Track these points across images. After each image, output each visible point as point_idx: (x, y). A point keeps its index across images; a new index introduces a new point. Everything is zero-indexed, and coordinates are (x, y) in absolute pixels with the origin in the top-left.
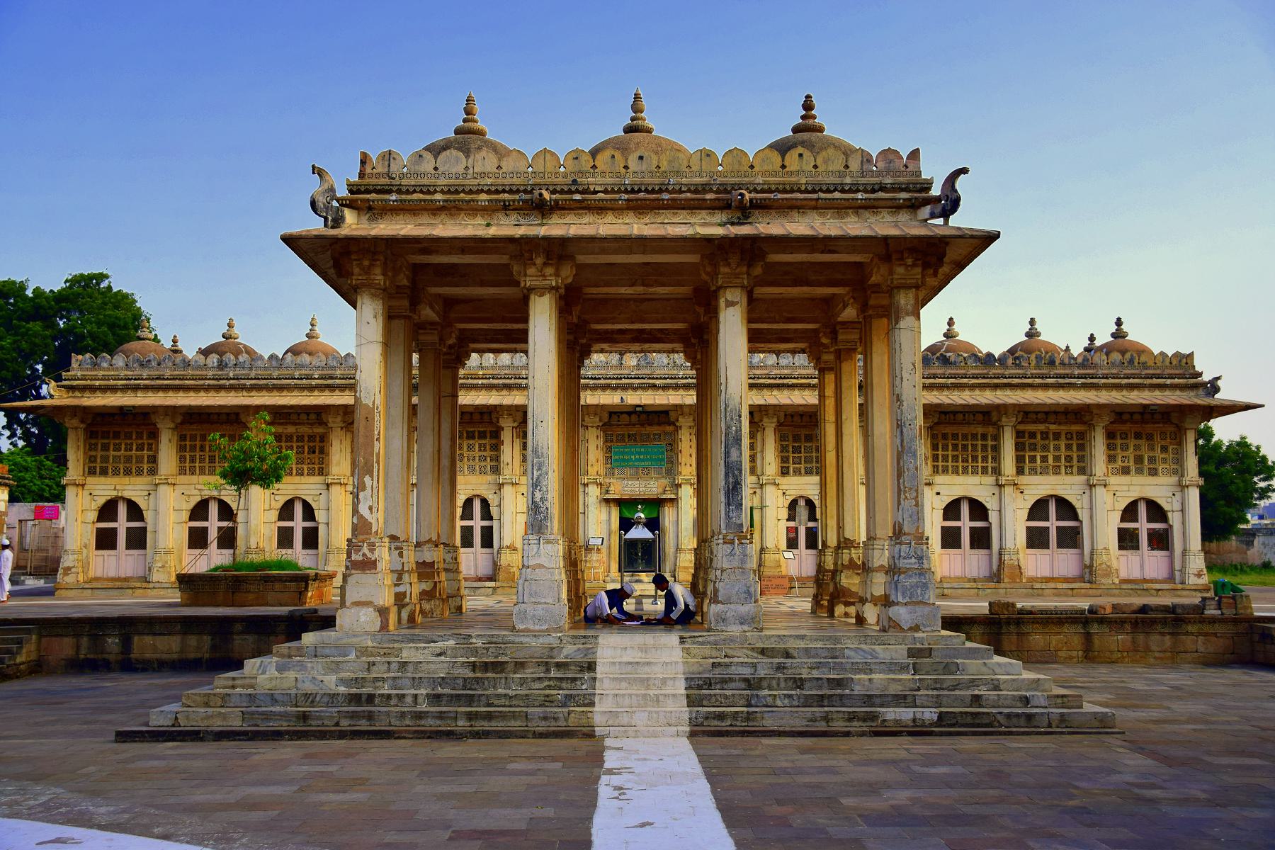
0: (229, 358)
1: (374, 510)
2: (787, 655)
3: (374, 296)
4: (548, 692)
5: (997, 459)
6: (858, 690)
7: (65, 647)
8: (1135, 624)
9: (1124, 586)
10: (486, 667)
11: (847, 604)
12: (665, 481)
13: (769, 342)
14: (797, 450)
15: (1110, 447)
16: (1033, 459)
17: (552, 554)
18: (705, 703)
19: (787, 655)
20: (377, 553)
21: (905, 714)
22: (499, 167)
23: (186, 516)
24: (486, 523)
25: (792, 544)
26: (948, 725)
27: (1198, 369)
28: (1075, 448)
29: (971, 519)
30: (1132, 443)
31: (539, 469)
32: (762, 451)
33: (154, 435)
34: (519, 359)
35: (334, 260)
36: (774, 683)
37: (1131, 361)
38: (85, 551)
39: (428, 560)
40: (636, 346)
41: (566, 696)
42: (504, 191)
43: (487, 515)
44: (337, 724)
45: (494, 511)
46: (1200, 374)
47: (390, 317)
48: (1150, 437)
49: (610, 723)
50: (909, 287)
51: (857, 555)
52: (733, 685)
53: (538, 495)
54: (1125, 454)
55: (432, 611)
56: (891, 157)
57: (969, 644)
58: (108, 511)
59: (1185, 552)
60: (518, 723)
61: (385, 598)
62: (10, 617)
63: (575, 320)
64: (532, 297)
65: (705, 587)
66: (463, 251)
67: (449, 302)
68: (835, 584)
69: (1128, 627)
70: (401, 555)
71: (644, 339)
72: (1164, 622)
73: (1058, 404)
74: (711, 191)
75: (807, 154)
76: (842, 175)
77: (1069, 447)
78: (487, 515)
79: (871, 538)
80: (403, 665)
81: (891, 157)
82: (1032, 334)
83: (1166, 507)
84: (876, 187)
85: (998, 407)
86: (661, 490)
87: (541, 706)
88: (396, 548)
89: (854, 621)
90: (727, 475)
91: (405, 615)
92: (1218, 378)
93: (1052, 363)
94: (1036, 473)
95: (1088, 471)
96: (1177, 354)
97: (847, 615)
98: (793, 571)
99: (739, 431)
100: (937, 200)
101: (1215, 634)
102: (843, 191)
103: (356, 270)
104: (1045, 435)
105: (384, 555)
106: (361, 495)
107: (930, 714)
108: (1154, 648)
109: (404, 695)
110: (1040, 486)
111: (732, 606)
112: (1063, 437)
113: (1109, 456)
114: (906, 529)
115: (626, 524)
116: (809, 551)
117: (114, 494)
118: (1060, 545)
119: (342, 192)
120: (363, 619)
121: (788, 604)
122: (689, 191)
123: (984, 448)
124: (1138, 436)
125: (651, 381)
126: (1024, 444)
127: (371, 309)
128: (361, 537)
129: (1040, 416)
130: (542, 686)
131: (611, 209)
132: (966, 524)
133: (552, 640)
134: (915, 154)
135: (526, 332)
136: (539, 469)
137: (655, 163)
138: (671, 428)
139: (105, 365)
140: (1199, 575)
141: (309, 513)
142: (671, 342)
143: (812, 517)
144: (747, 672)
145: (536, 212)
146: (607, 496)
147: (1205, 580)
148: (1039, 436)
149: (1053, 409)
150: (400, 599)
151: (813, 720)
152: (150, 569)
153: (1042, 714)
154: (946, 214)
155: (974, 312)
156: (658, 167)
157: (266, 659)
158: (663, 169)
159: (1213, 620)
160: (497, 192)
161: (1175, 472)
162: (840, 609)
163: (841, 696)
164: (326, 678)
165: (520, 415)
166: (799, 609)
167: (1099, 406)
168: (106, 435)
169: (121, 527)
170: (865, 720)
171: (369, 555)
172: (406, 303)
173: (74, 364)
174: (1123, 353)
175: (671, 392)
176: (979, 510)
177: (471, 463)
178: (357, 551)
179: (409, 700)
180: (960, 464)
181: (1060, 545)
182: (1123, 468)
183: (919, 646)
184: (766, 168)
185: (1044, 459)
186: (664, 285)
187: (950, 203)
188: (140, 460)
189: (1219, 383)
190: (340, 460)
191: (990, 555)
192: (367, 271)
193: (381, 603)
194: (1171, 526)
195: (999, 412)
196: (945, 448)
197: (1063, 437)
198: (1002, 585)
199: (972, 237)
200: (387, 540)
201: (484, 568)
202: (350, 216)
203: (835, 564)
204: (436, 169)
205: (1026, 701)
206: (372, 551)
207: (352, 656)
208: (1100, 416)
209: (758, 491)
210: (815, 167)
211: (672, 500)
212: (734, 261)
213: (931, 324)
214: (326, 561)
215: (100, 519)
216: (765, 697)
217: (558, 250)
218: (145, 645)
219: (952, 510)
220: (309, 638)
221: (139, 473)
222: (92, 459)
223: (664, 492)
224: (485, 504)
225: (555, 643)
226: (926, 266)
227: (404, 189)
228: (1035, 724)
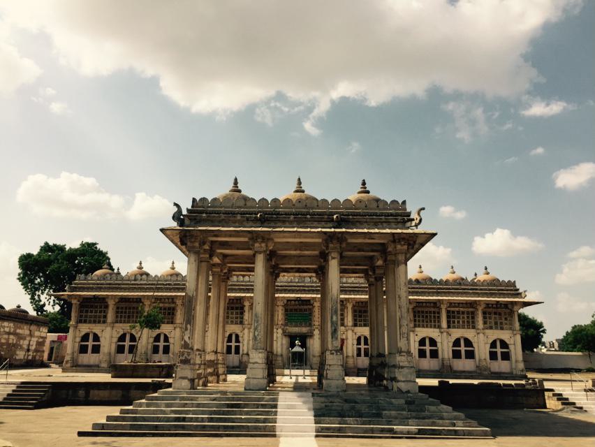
16: (454, 322)
20: (190, 356)
22: (245, 205)
24: (237, 344)
27: (518, 287)
30: (493, 316)
45: (241, 339)
46: (518, 290)
48: (500, 314)
59: (516, 361)
66: (230, 236)
67: (225, 256)
70: (201, 357)
77: (468, 317)
78: (237, 340)
88: (199, 354)
99: (337, 308)
104: (458, 312)
118: (466, 358)
119: (185, 212)
120: (183, 384)
123: (434, 317)
124: (495, 313)
134: (404, 202)
138: (311, 307)
168: (87, 307)
172: (208, 256)
181: (466, 358)
185: (458, 322)
186: (307, 250)
196: (419, 317)
222: (81, 316)
224: (237, 336)
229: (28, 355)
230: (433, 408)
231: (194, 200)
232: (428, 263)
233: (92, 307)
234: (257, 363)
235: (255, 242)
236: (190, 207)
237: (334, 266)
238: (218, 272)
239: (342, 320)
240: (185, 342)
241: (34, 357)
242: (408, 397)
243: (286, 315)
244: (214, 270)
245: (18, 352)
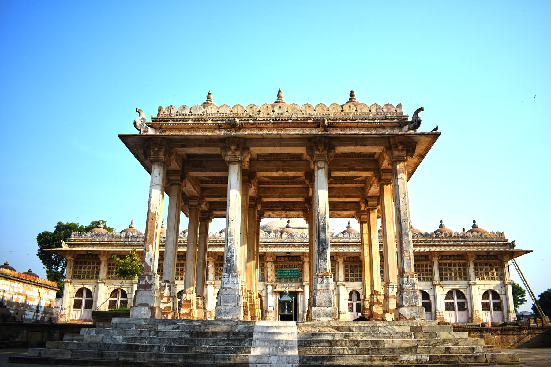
0: (130, 234)
1: (152, 260)
2: (350, 330)
3: (159, 165)
5: (432, 274)
10: (198, 334)
12: (298, 284)
13: (339, 210)
14: (352, 271)
15: (476, 269)
16: (446, 275)
27: (506, 238)
28: (462, 270)
30: (484, 267)
32: (338, 272)
33: (99, 263)
36: (344, 343)
37: (481, 235)
44: (118, 359)
46: (507, 240)
48: (491, 265)
49: (258, 361)
52: (322, 344)
54: (482, 272)
56: (389, 107)
60: (210, 361)
67: (211, 203)
76: (367, 113)
77: (460, 269)
80: (157, 332)
81: (389, 107)
82: (441, 226)
84: (384, 118)
85: (431, 253)
87: (223, 353)
90: (319, 245)
92: (514, 241)
93: (451, 236)
94: (448, 280)
96: (498, 232)
100: (412, 122)
102: (369, 120)
103: (152, 153)
104: (450, 265)
108: (510, 341)
109: (153, 346)
111: (323, 308)
113: (476, 273)
120: (143, 312)
123: (427, 270)
124: (486, 265)
128: (145, 273)
129: (448, 257)
130: (225, 344)
134: (399, 106)
136: (230, 242)
137: (286, 110)
138: (301, 263)
139: (83, 236)
142: (298, 211)
143: (359, 299)
144: (329, 338)
149: (452, 254)
151: (364, 361)
153: (482, 356)
156: (287, 111)
158: (289, 112)
159: (534, 328)
160: (216, 121)
163: (378, 349)
164: (118, 337)
167: (470, 252)
168: (81, 263)
170: (391, 361)
171: (148, 281)
172: (179, 178)
173: (72, 236)
174: (478, 232)
175: (301, 248)
178: (143, 280)
179: (156, 348)
184: (334, 111)
185: (450, 274)
186: (291, 171)
187: (417, 123)
188: (93, 273)
189: (515, 243)
191: (431, 314)
192: (157, 153)
194: (502, 301)
195: (432, 256)
204: (190, 112)
205: (473, 350)
206: (150, 280)
207: (134, 328)
208: (471, 256)
209: (337, 288)
210: (356, 111)
211: (301, 292)
212: (321, 148)
216: (339, 349)
221: (92, 278)
222: (75, 272)
226: (408, 151)
228: (479, 361)
229: (37, 316)
233: (85, 263)
234: (229, 288)
235: (227, 152)
238: (196, 206)
241: (43, 318)
243: (276, 271)
244: (191, 203)
245: (27, 312)
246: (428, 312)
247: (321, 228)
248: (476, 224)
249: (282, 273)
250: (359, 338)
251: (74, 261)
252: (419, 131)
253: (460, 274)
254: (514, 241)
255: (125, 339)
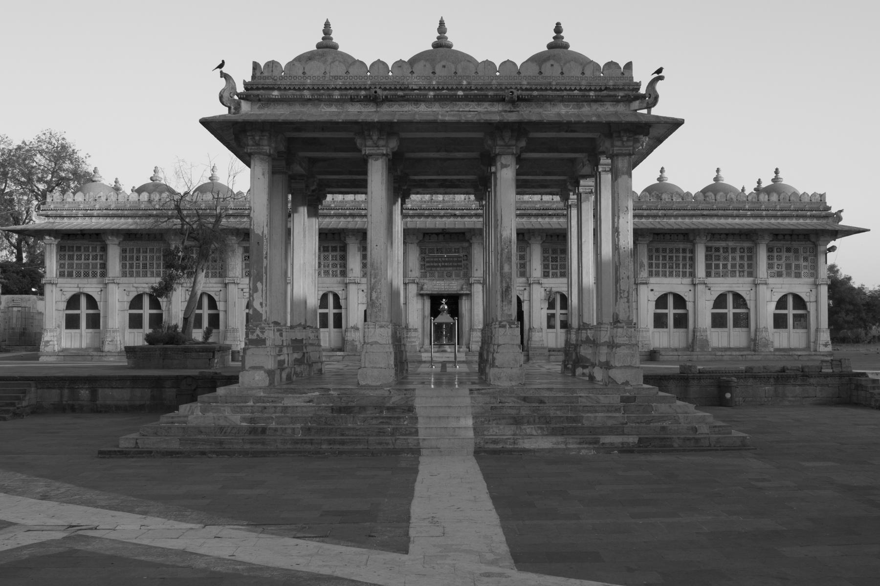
2: (542, 402)
3: (262, 160)
4: (381, 426)
5: (693, 266)
6: (586, 423)
7: (52, 396)
8: (777, 379)
9: (777, 353)
10: (340, 410)
11: (584, 367)
12: (462, 282)
15: (770, 258)
16: (717, 266)
17: (383, 335)
18: (486, 433)
19: (542, 402)
20: (266, 335)
21: (617, 440)
22: (347, 72)
23: (127, 305)
24: (336, 311)
25: (550, 326)
26: (645, 446)
28: (746, 259)
29: (675, 308)
30: (784, 254)
31: (375, 277)
34: (361, 197)
35: (230, 132)
38: (58, 330)
39: (299, 338)
40: (442, 190)
41: (393, 429)
42: (351, 89)
43: (337, 305)
45: (342, 302)
46: (829, 208)
47: (274, 172)
48: (796, 251)
50: (625, 155)
51: (590, 333)
53: (374, 295)
54: (779, 262)
55: (301, 373)
57: (661, 394)
58: (73, 302)
59: (817, 330)
61: (270, 364)
62: (16, 375)
63: (399, 173)
64: (370, 161)
65: (488, 356)
66: (323, 130)
67: (313, 161)
68: (576, 353)
69: (772, 380)
70: (281, 335)
71: (449, 187)
72: (796, 377)
73: (735, 229)
74: (491, 89)
75: (556, 65)
77: (742, 258)
78: (337, 305)
79: (600, 323)
80: (285, 409)
83: (806, 299)
86: (459, 288)
88: (278, 330)
89: (587, 378)
90: (501, 282)
91: (284, 375)
92: (841, 211)
95: (754, 274)
97: (584, 375)
98: (552, 344)
99: (510, 252)
100: (643, 97)
101: (828, 385)
103: (250, 142)
104: (726, 250)
105: (270, 335)
106: (255, 295)
107: (633, 440)
109: (286, 429)
110: (722, 285)
112: (738, 251)
114: (621, 317)
115: (435, 312)
116: (336, 330)
117: (77, 290)
119: (240, 89)
120: (257, 378)
121: (547, 367)
122: (476, 89)
123: (684, 258)
124: (788, 250)
125: (452, 212)
126: (711, 256)
127: (261, 167)
131: (424, 101)
132: (671, 311)
133: (384, 392)
134: (629, 66)
135: (366, 181)
136: (375, 277)
137: (453, 70)
138: (466, 245)
140: (826, 345)
141: (213, 304)
144: (513, 412)
145: (372, 104)
146: (422, 292)
147: (829, 348)
148: (721, 250)
150: (281, 363)
151: (558, 443)
152: (103, 343)
153: (705, 438)
154: (649, 107)
155: (678, 166)
156: (456, 73)
157: (193, 405)
159: (827, 376)
161: (812, 275)
162: (579, 371)
165: (362, 235)
166: (553, 370)
168: (71, 249)
169: (83, 312)
176: (680, 301)
177: (327, 269)
178: (253, 333)
180: (668, 270)
182: (778, 272)
183: (628, 394)
185: (725, 266)
186: (459, 151)
187: (652, 99)
189: (842, 214)
190: (236, 265)
191: (687, 333)
193: (270, 367)
194: (809, 312)
196: (657, 258)
197: (738, 251)
198: (695, 353)
199: (666, 123)
200: (272, 325)
201: (335, 343)
202: (245, 107)
203: (577, 340)
206: (263, 332)
211: (467, 295)
213: (643, 177)
214: (225, 338)
215: (68, 308)
217: (387, 129)
218: (107, 395)
219: (661, 302)
220: (221, 391)
223: (462, 289)
224: (336, 297)
225: (387, 394)
227: (283, 87)
230: (663, 408)
231: (256, 66)
232: (678, 166)
234: (376, 343)
236: (249, 79)
237: (506, 175)
239: (523, 266)
240: (255, 310)
242: (625, 391)
243: (423, 259)
246: (682, 330)
247: (504, 256)
248: (780, 175)
249: (433, 262)
250: (552, 413)
251: (57, 245)
252: (655, 111)
253: (742, 266)
254: (841, 211)
255: (244, 419)
